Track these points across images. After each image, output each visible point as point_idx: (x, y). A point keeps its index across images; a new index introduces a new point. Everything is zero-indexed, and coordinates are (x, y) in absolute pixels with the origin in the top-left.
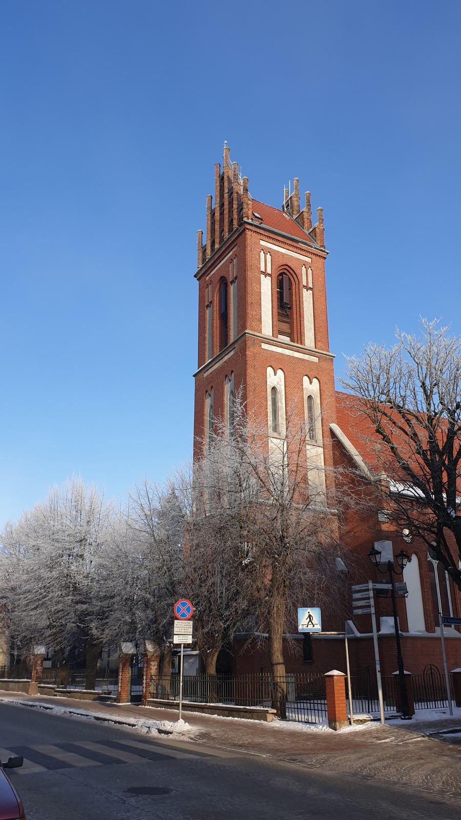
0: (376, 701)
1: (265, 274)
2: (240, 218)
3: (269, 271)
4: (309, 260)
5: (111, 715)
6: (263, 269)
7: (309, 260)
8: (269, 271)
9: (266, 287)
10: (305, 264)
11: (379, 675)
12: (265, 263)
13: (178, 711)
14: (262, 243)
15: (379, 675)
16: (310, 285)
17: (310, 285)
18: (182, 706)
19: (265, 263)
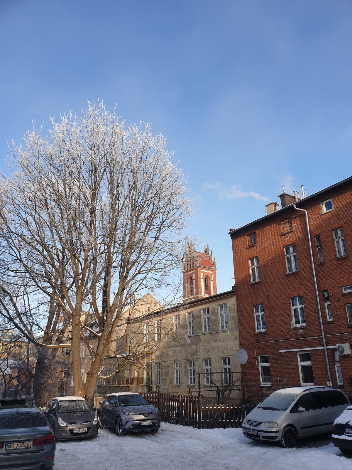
0: (296, 321)
1: (202, 279)
2: (177, 318)
3: (203, 278)
4: (212, 272)
5: (14, 405)
6: (202, 278)
7: (212, 272)
8: (203, 278)
9: (202, 282)
10: (211, 274)
11: (197, 414)
12: (202, 276)
13: (328, 347)
14: (201, 270)
15: (197, 414)
16: (213, 280)
17: (213, 280)
18: (265, 382)
19: (202, 276)
